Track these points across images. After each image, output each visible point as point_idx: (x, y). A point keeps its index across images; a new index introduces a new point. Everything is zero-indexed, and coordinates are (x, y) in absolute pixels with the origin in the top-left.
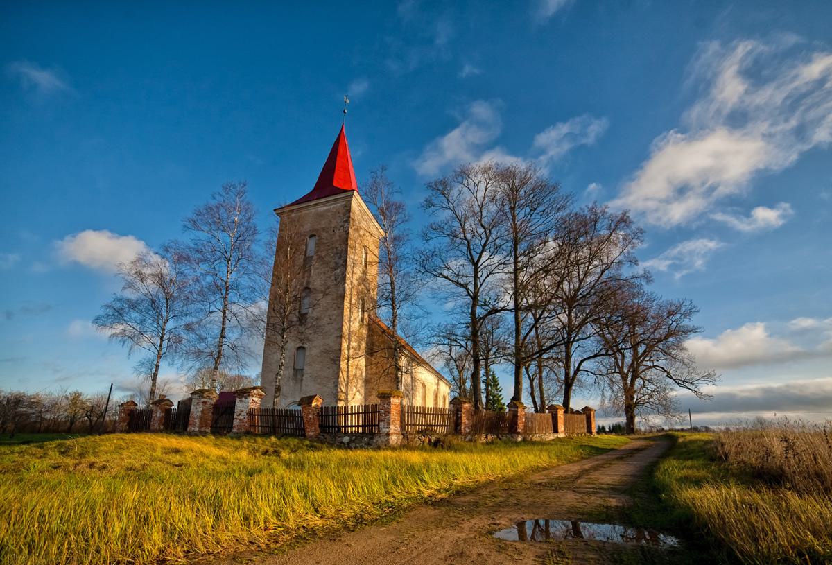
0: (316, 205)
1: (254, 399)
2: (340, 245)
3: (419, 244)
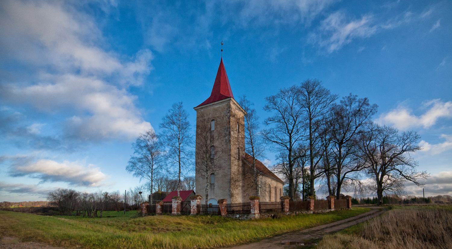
0: (213, 105)
1: (198, 200)
2: (226, 124)
3: (263, 127)
